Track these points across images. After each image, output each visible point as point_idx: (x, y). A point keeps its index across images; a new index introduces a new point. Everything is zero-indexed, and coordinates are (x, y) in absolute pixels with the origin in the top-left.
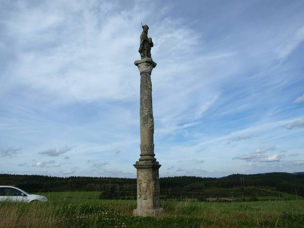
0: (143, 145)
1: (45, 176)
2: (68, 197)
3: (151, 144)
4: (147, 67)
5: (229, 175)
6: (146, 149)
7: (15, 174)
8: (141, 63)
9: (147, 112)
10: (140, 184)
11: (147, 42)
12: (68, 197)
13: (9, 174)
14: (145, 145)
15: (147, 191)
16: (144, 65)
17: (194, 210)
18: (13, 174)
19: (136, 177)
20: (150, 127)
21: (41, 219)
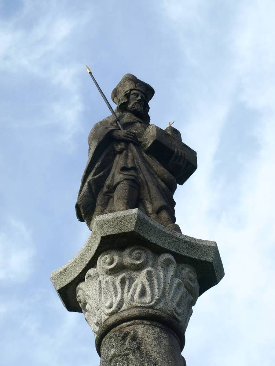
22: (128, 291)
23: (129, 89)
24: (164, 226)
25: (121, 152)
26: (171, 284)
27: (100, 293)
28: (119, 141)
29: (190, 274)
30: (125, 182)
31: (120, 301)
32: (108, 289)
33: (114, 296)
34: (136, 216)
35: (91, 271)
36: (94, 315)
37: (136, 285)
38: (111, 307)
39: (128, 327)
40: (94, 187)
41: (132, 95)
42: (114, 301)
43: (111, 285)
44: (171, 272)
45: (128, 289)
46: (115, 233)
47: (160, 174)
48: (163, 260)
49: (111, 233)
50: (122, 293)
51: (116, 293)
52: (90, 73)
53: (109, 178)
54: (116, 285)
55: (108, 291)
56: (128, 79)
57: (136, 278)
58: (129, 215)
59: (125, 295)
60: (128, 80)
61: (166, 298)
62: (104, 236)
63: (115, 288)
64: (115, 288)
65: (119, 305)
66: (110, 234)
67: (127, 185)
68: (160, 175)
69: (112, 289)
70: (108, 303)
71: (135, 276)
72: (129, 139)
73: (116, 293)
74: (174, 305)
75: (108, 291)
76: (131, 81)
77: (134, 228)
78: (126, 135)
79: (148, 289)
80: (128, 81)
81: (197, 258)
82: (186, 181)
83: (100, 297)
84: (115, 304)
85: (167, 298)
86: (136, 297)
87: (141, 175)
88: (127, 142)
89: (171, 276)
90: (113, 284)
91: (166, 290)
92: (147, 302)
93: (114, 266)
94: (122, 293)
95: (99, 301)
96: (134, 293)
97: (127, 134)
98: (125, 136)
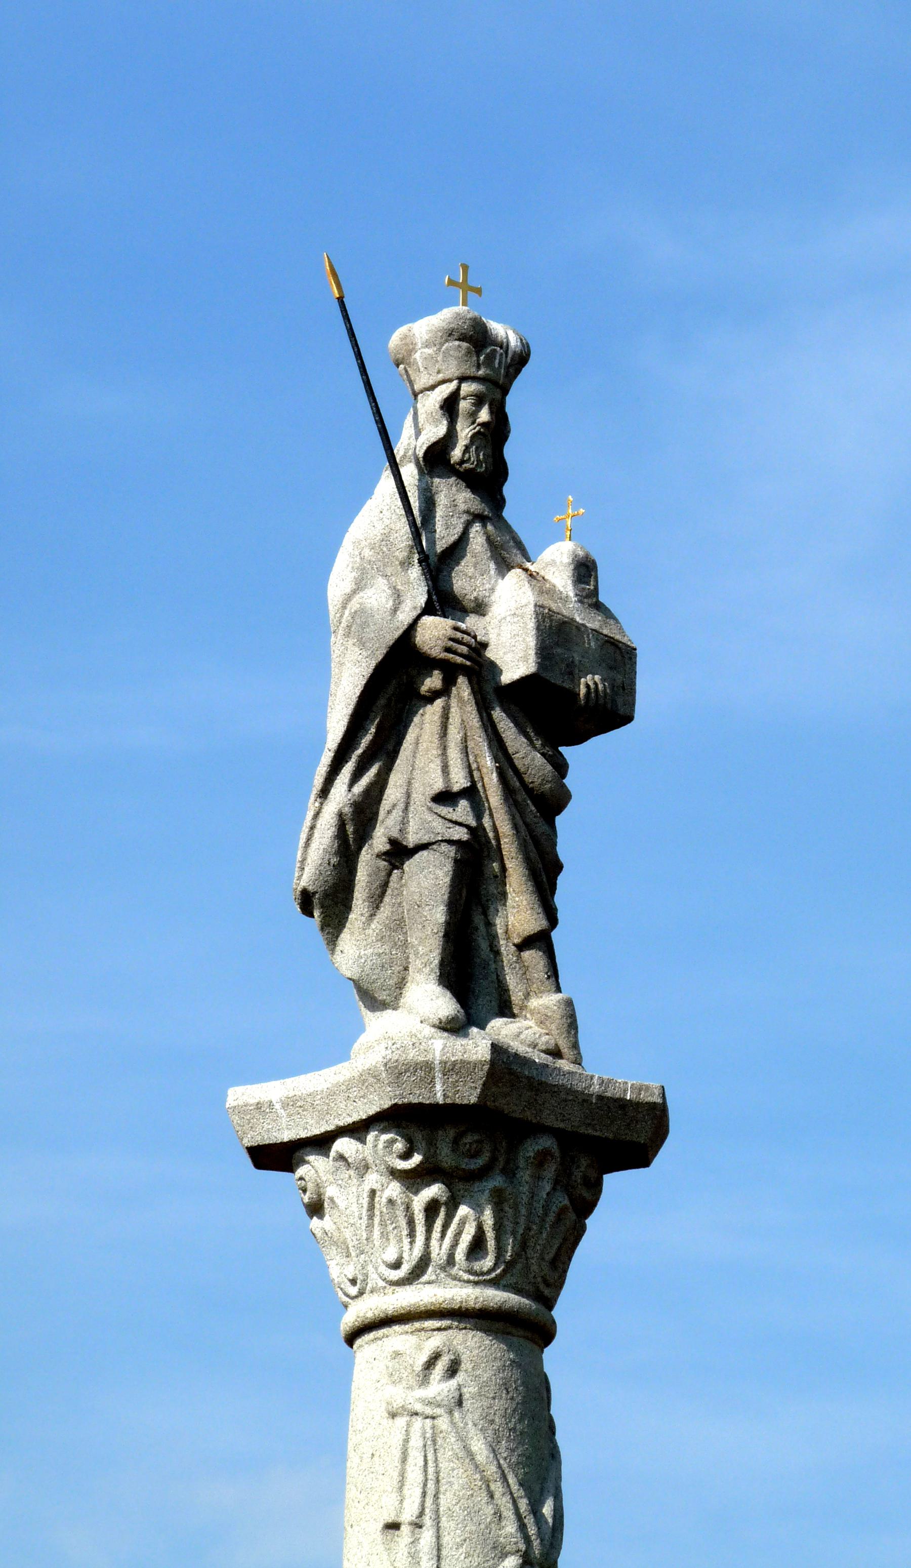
22: (442, 1237)
23: (456, 375)
26: (546, 1208)
27: (371, 1217)
28: (428, 664)
29: (508, 556)
30: (444, 847)
31: (421, 1259)
33: (406, 1241)
34: (486, 1067)
35: (343, 1145)
36: (344, 1254)
37: (463, 1222)
39: (436, 1332)
40: (351, 830)
41: (464, 398)
42: (406, 1256)
43: (400, 1213)
44: (545, 1182)
45: (442, 1231)
46: (428, 1102)
47: (532, 782)
48: (532, 1154)
49: (421, 1101)
50: (428, 1239)
51: (412, 1234)
52: (341, 300)
54: (413, 1214)
55: (394, 1225)
56: (456, 335)
57: (463, 1197)
58: (469, 1063)
59: (434, 1243)
60: (456, 340)
61: (528, 1252)
62: (400, 1102)
63: (411, 1223)
64: (411, 1223)
65: (416, 1269)
66: (416, 1101)
68: (531, 786)
69: (403, 1223)
70: (391, 1255)
71: (462, 1192)
72: (459, 660)
73: (412, 1234)
74: (543, 1268)
75: (394, 1225)
76: (465, 345)
77: (478, 1098)
78: (451, 643)
79: (491, 1244)
80: (457, 343)
81: (611, 1136)
84: (410, 1263)
85: (531, 1254)
86: (460, 1254)
89: (545, 1196)
90: (407, 1211)
91: (530, 1234)
92: (485, 1269)
93: (413, 1166)
94: (428, 1239)
95: (367, 1239)
97: (451, 639)
98: (448, 650)
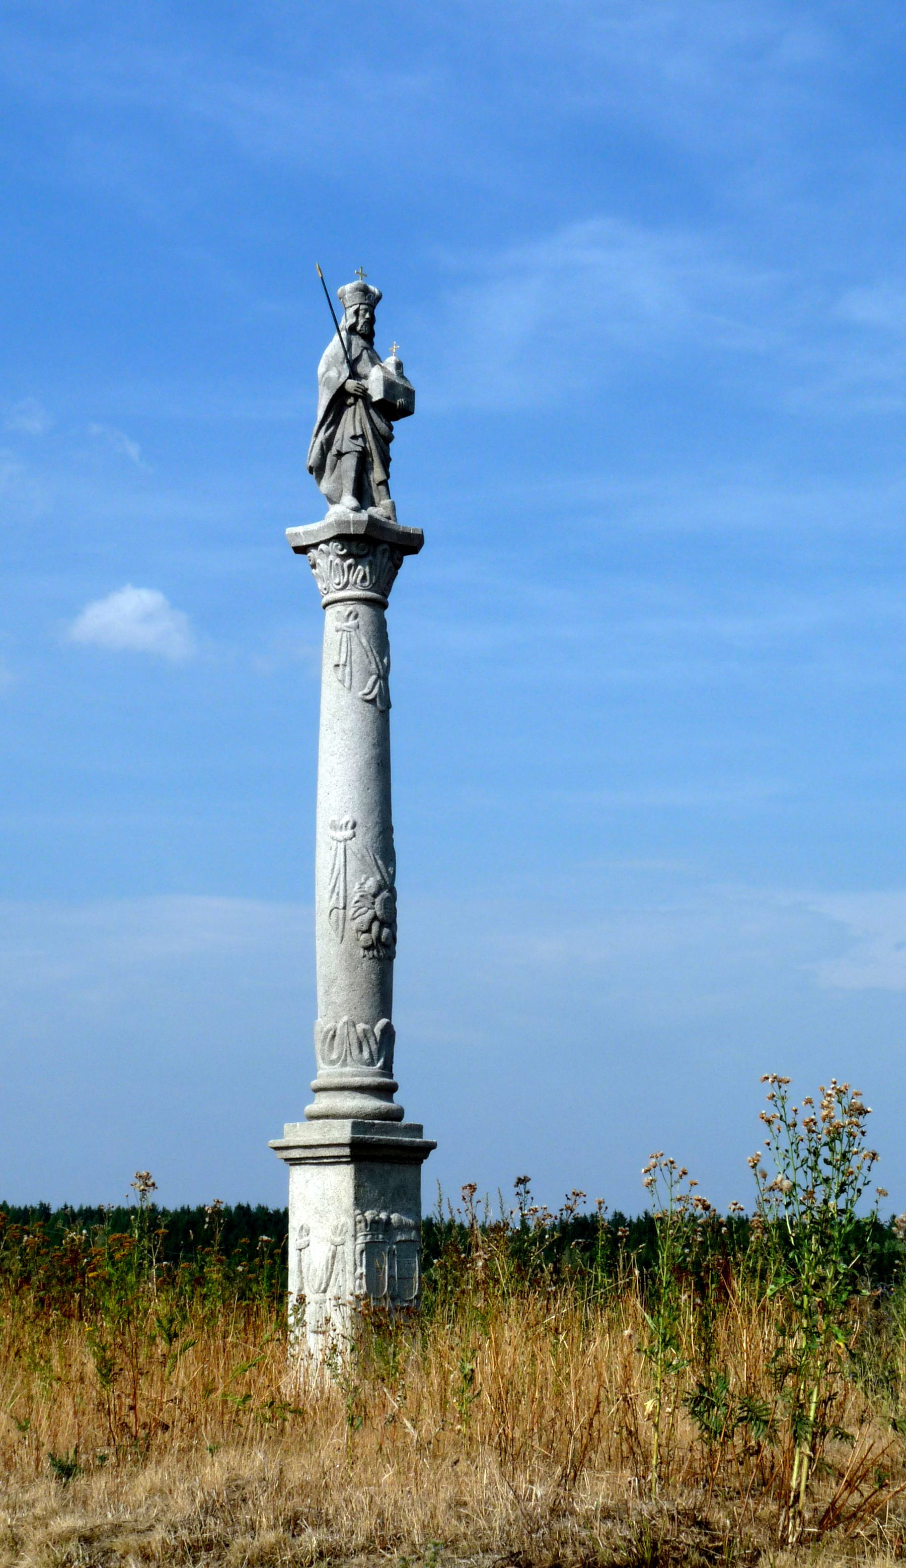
0: (325, 1030)
1: (233, 1209)
2: (844, 1400)
3: (361, 1027)
4: (350, 567)
5: (90, 1208)
6: (334, 1056)
7: (46, 1201)
8: (315, 546)
9: (346, 840)
10: (300, 1250)
11: (354, 404)
12: (844, 1400)
13: (22, 1208)
14: (332, 1033)
15: (328, 1285)
16: (331, 557)
17: (164, 1355)
18: (36, 1205)
19: (845, 1208)
20: (357, 931)
21: (264, 1520)
24: (354, 1537)
25: (350, 406)
27: (331, 569)
28: (349, 395)
32: (338, 569)
35: (322, 546)
38: (339, 584)
50: (349, 576)
51: (343, 575)
53: (302, 1299)
59: (350, 577)
67: (342, 759)
69: (341, 571)
70: (337, 581)
79: (368, 578)
82: (391, 1003)
83: (330, 572)
87: (367, 445)
88: (356, 398)
94: (349, 576)
96: (357, 577)
98: (355, 390)
